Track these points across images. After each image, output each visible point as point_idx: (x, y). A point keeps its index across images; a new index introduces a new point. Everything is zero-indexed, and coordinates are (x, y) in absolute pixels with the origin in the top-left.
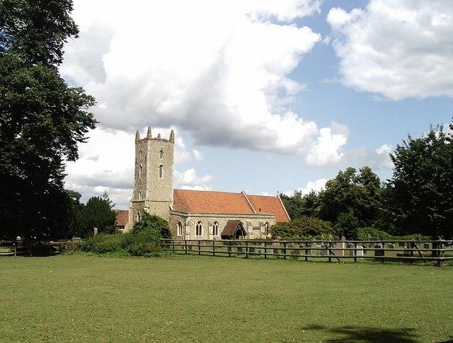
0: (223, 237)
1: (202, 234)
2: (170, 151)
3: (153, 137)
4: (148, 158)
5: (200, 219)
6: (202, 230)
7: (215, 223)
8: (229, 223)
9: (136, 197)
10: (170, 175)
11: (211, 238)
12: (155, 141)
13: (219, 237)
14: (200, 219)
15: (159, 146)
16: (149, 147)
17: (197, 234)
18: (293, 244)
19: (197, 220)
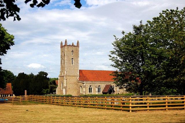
0: (103, 93)
1: (92, 92)
2: (77, 51)
3: (63, 45)
4: (66, 55)
5: (90, 84)
6: (92, 90)
7: (90, 86)
8: (107, 86)
9: (61, 74)
10: (77, 63)
11: (97, 93)
12: (70, 47)
13: (101, 93)
14: (90, 84)
15: (71, 49)
16: (66, 50)
17: (89, 92)
18: (82, 97)
19: (89, 85)
